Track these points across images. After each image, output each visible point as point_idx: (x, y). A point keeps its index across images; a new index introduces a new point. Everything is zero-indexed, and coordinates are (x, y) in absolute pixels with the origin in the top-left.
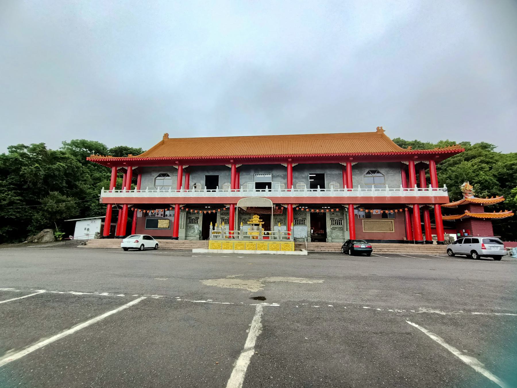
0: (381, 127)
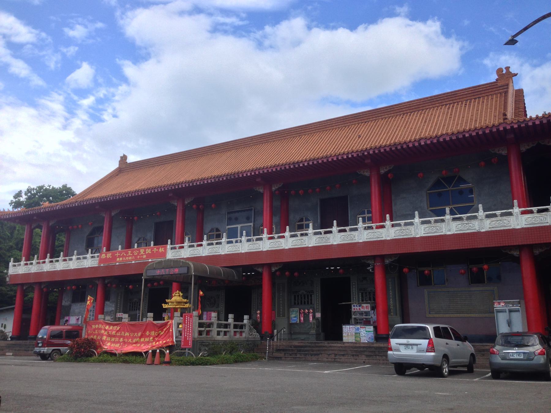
0: (508, 68)
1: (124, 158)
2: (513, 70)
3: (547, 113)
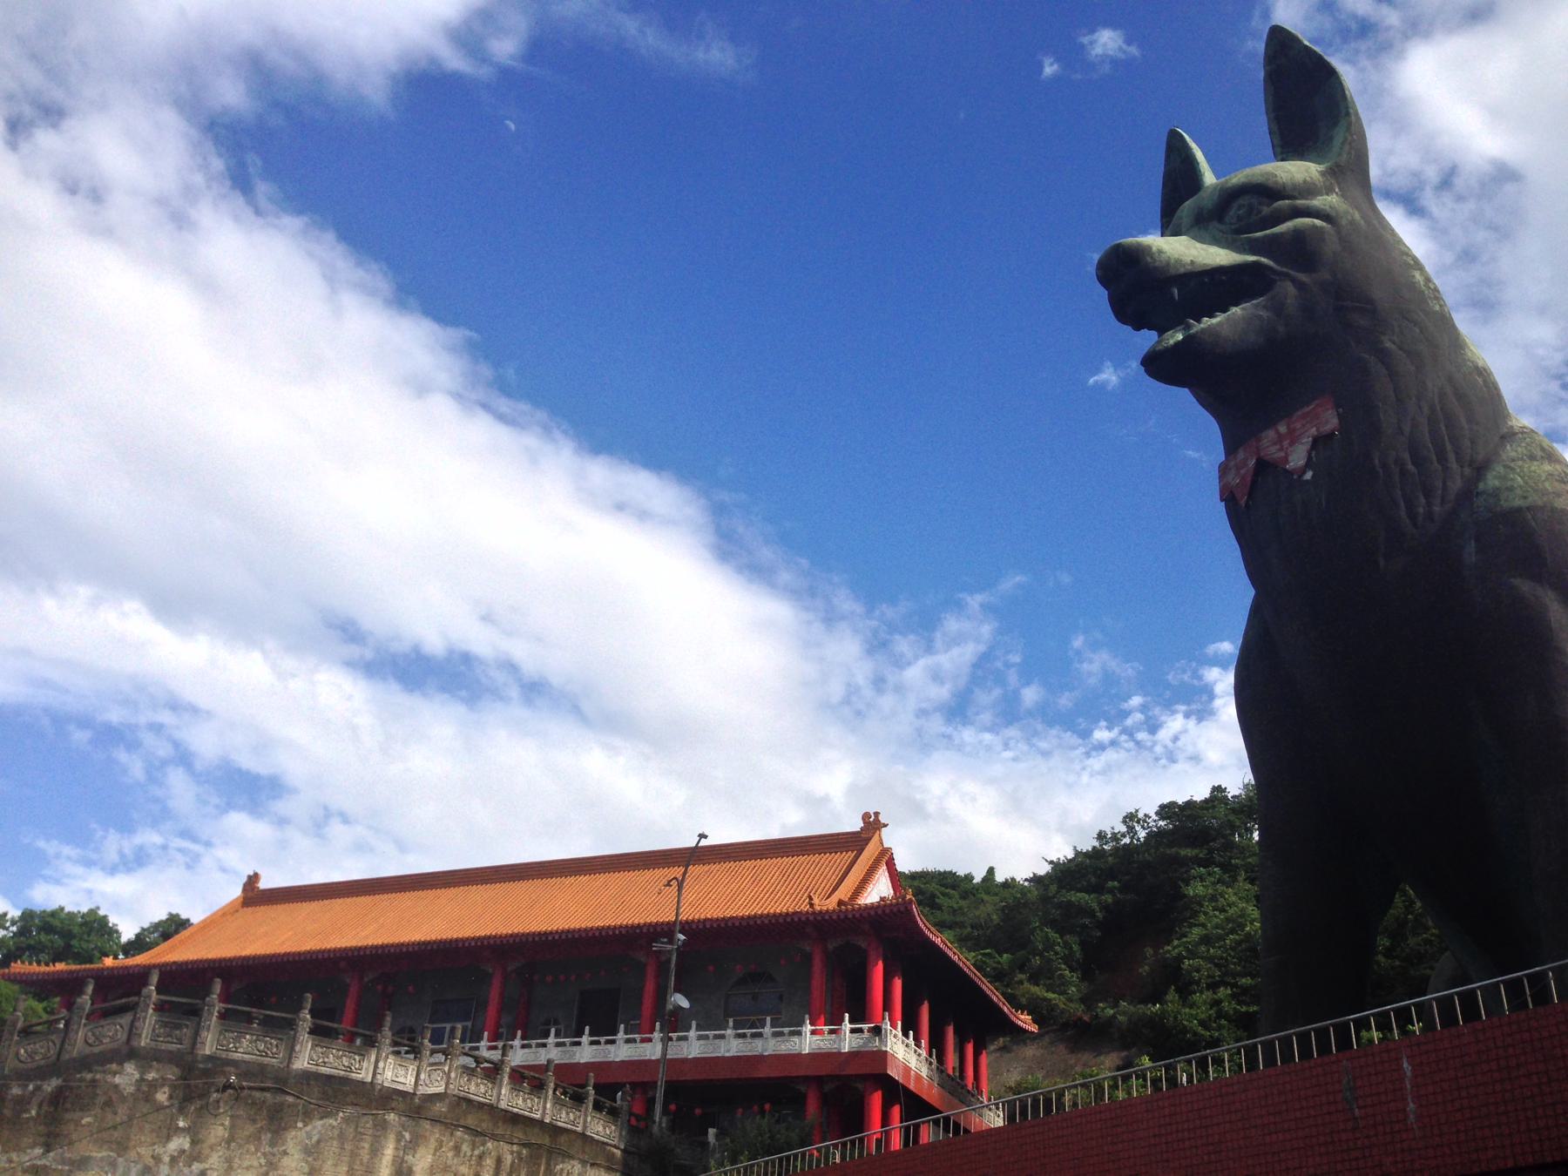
0: (877, 814)
1: (253, 879)
2: (882, 819)
3: (1000, 878)
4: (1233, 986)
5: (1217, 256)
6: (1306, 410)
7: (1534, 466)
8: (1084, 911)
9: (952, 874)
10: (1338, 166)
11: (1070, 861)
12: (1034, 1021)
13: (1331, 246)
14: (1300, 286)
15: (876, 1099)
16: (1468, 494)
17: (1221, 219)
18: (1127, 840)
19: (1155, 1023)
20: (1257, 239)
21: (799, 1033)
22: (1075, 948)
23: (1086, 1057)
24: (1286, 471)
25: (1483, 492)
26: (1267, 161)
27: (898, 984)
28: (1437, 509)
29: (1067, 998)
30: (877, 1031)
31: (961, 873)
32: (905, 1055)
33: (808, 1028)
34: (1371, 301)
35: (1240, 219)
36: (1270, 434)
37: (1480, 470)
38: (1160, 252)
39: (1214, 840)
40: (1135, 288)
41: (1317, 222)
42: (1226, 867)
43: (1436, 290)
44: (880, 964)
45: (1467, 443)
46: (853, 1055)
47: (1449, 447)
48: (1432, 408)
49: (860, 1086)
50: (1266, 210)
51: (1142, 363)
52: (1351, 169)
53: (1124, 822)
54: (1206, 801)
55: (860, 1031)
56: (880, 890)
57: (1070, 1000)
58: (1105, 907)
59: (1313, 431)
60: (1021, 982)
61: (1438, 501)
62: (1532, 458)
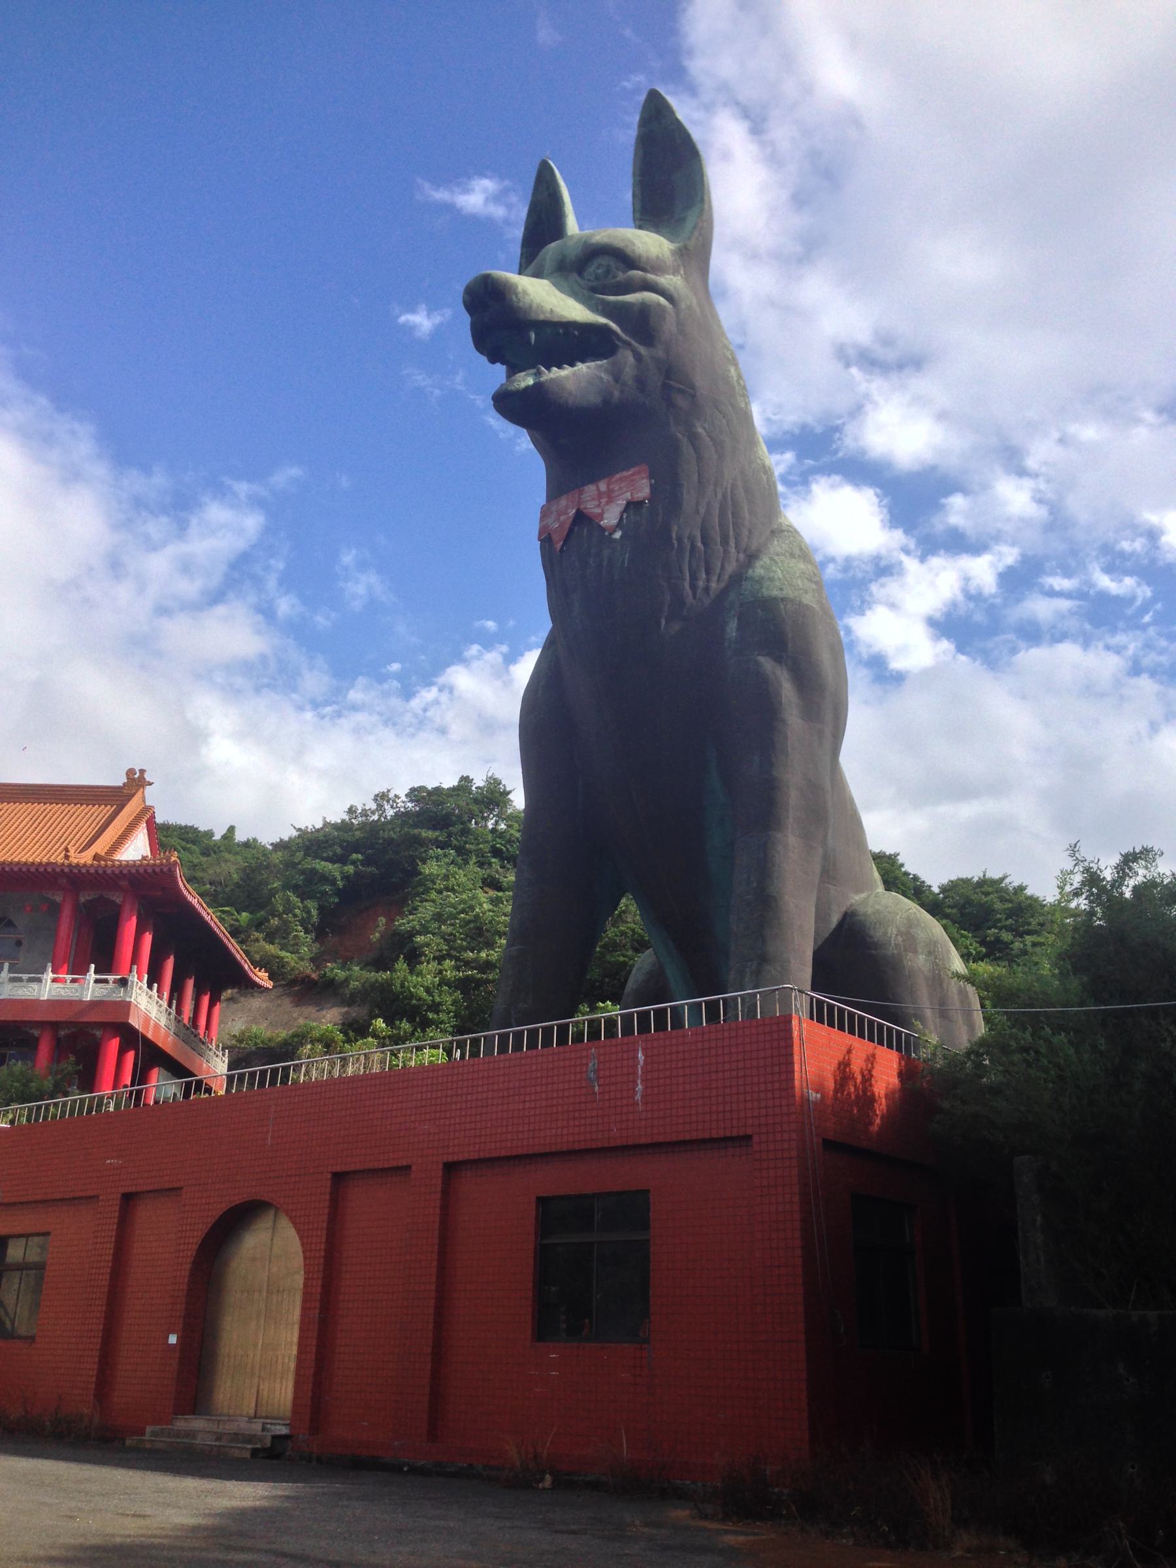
0: (142, 771)
2: (148, 777)
3: (240, 837)
4: (457, 959)
5: (574, 310)
6: (625, 474)
7: (793, 563)
8: (325, 878)
9: (194, 830)
10: (686, 247)
11: (318, 831)
12: (270, 978)
13: (669, 326)
14: (638, 357)
15: (114, 1044)
16: (738, 579)
17: (580, 273)
18: (376, 817)
19: (385, 987)
20: (608, 303)
21: (39, 980)
22: (314, 912)
23: (311, 1010)
24: (600, 526)
25: (751, 578)
26: (627, 226)
27: (148, 938)
28: (713, 585)
29: (299, 957)
30: (123, 982)
31: (203, 828)
32: (148, 1007)
33: (49, 975)
34: (693, 387)
35: (597, 278)
36: (591, 489)
37: (752, 558)
38: (525, 292)
39: (453, 825)
40: (495, 321)
41: (662, 300)
42: (461, 851)
43: (744, 387)
44: (134, 919)
45: (745, 532)
46: (95, 1004)
47: (731, 533)
48: (724, 497)
49: (98, 1033)
50: (621, 276)
51: (493, 398)
52: (696, 256)
53: (375, 800)
54: (454, 789)
55: (106, 981)
56: (137, 849)
57: (302, 959)
58: (346, 877)
59: (628, 495)
60: (257, 940)
61: (716, 578)
62: (792, 555)
